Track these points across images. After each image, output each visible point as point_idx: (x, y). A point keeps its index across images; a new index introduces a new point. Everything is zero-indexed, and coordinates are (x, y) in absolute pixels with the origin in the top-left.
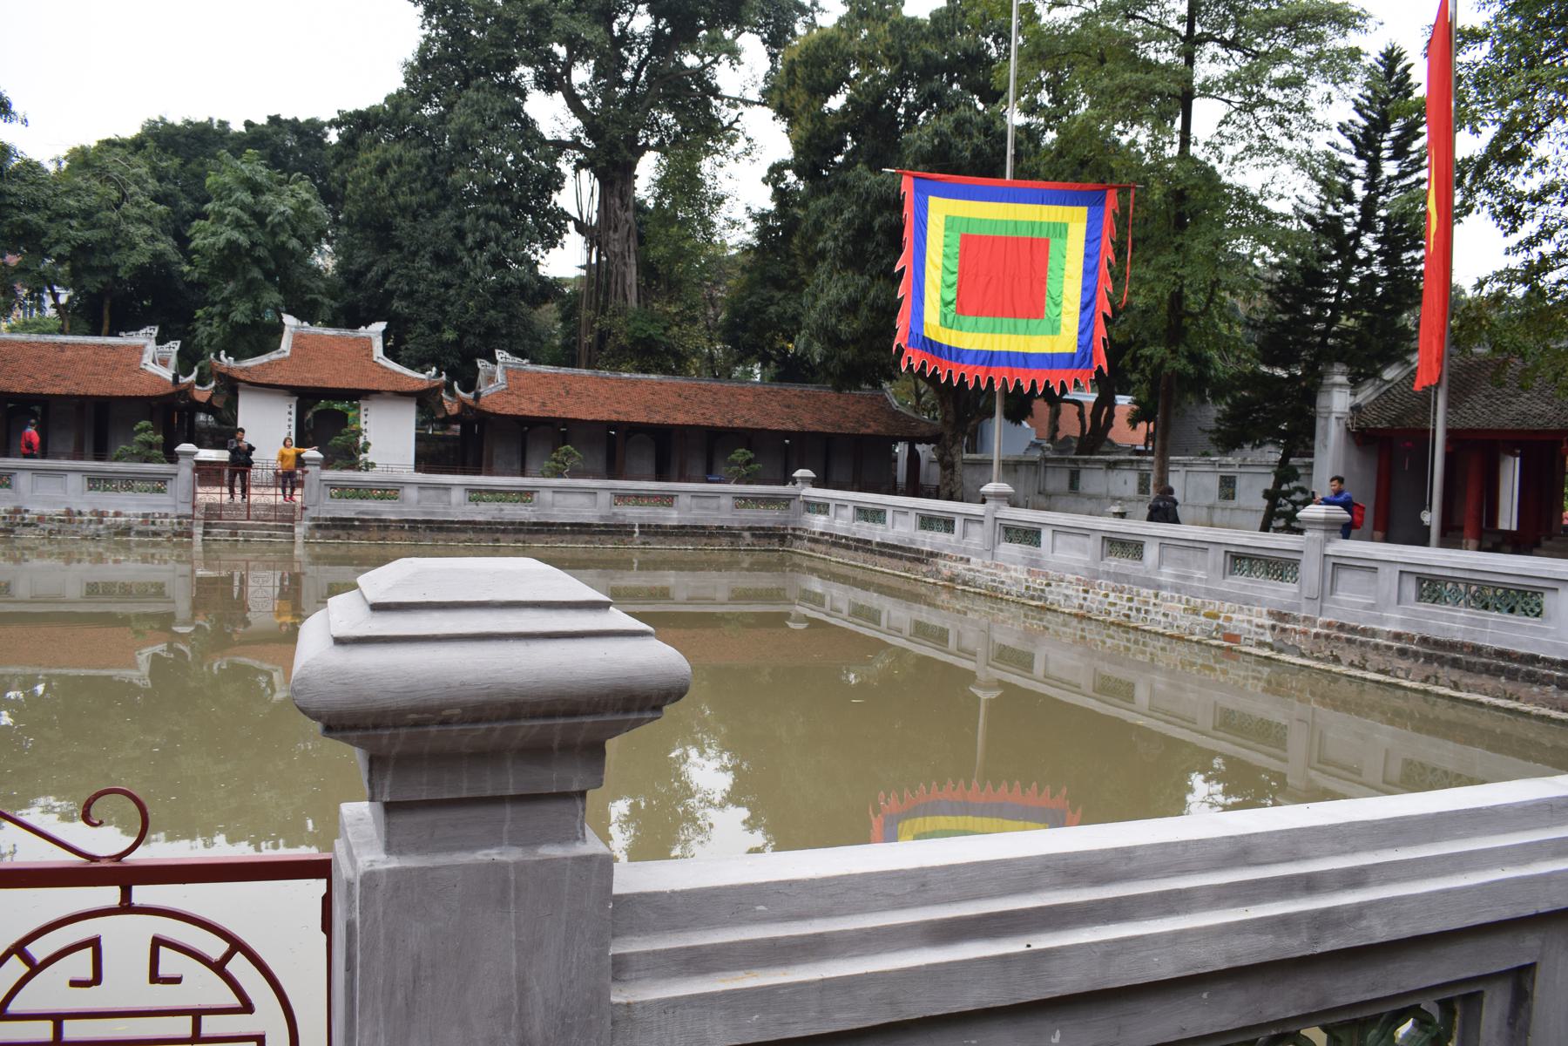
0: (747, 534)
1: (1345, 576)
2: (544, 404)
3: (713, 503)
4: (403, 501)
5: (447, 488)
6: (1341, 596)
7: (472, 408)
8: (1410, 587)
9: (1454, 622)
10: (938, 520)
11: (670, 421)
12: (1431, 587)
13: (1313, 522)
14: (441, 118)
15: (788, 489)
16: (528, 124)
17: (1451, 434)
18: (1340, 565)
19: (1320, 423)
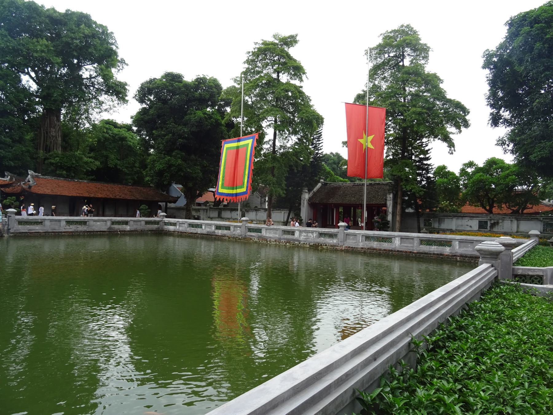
0: (149, 232)
1: (348, 236)
2: (52, 190)
3: (139, 223)
4: (45, 226)
5: (60, 221)
6: (348, 241)
7: (27, 191)
8: (364, 238)
9: (375, 245)
10: (223, 227)
11: (97, 196)
12: (368, 238)
13: (341, 226)
14: (292, 92)
15: (156, 219)
16: (35, 74)
17: (367, 204)
18: (347, 234)
19: (302, 201)
